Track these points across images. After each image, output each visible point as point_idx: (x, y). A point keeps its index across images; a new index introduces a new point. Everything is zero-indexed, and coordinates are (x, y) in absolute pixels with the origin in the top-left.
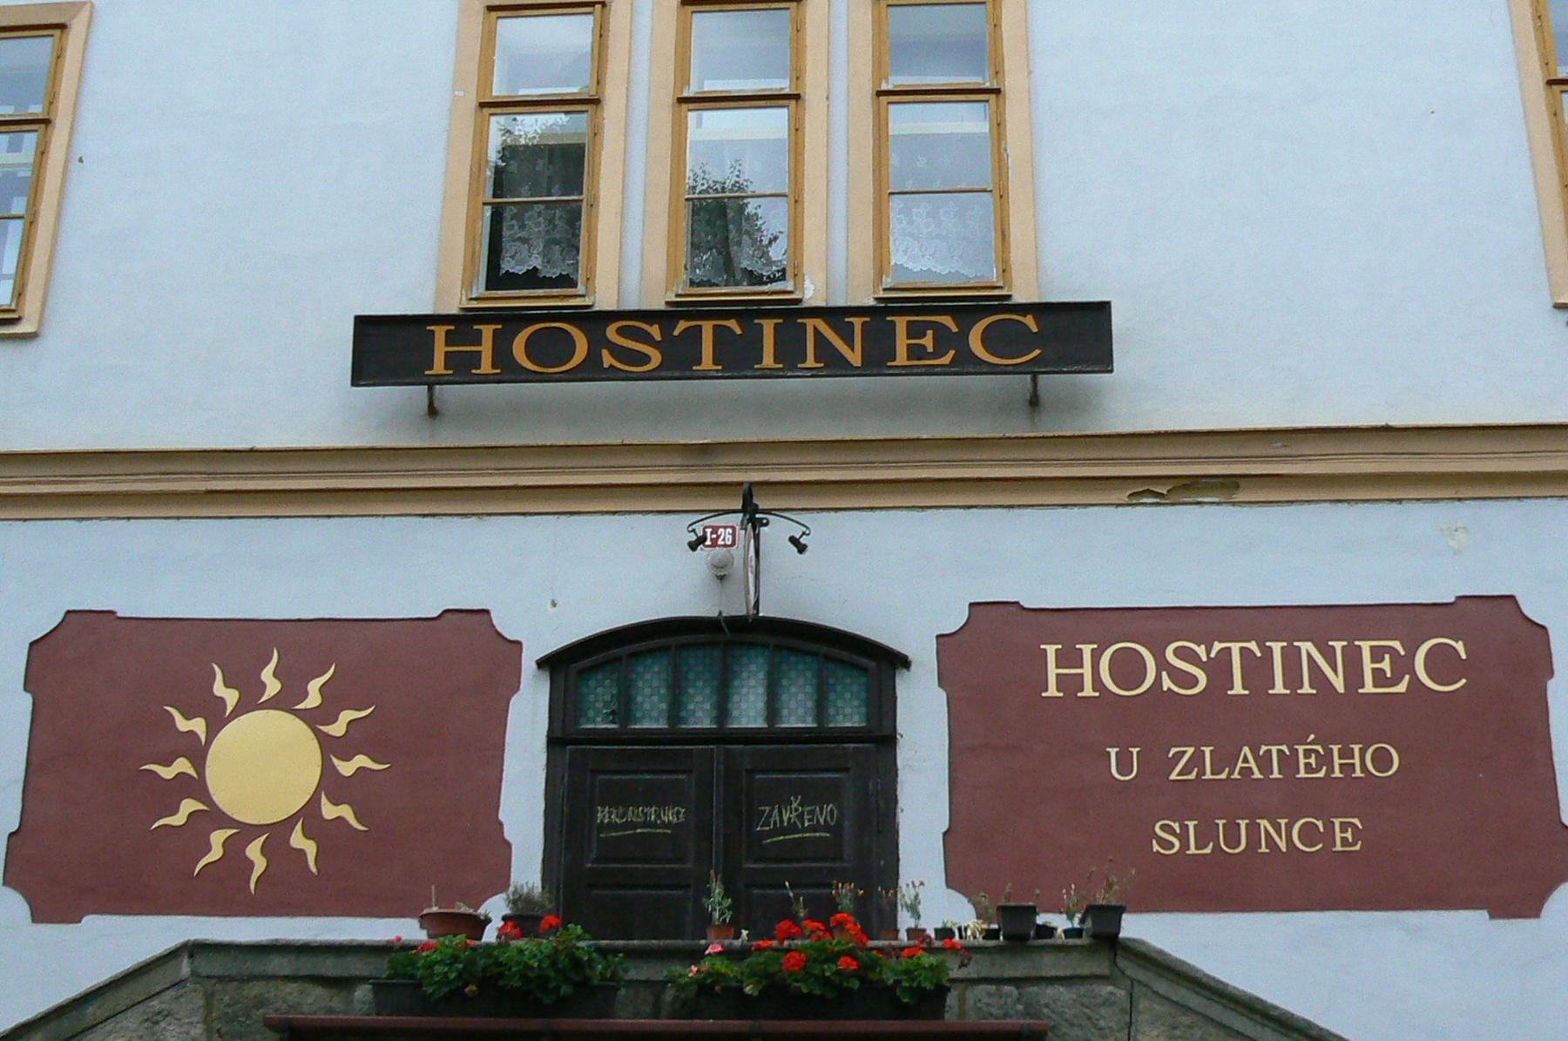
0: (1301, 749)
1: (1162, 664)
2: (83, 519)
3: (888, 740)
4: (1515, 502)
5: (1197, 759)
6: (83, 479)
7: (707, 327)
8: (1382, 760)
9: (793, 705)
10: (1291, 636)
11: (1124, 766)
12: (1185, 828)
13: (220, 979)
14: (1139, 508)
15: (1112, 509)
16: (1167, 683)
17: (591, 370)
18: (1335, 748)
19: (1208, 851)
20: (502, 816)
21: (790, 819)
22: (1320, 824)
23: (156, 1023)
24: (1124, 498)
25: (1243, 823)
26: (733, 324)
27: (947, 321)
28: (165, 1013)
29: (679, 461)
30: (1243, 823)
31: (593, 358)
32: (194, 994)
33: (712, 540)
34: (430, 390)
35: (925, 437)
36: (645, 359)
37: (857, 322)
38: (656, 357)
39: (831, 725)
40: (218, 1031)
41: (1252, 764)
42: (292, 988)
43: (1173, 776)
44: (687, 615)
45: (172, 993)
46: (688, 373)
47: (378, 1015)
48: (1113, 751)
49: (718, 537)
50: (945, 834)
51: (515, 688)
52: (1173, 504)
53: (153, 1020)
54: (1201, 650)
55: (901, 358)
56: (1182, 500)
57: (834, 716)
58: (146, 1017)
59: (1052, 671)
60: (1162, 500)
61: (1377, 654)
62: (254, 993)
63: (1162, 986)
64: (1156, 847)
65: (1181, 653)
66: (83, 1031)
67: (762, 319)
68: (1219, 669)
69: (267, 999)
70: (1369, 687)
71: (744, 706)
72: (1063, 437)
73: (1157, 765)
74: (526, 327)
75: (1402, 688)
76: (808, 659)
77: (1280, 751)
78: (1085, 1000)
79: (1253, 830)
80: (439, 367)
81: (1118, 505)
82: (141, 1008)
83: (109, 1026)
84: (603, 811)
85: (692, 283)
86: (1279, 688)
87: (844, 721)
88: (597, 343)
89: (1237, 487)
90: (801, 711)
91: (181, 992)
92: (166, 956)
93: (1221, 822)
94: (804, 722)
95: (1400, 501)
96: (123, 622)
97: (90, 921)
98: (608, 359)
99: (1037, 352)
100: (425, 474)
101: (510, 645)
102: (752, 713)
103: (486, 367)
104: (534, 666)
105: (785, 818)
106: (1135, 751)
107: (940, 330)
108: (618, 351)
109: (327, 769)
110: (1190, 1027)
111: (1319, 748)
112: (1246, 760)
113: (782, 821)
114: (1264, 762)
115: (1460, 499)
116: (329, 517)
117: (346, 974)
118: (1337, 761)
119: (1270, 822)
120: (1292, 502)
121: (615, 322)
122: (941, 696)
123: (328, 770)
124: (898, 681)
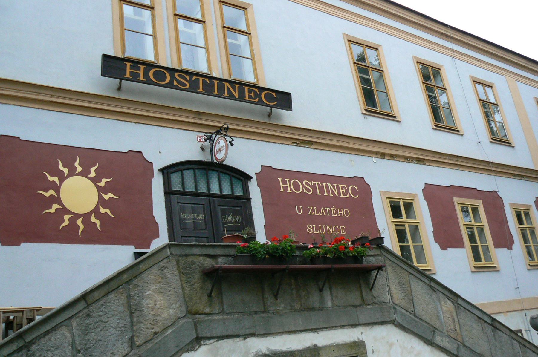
0: (332, 209)
1: (303, 186)
2: (4, 103)
3: (249, 199)
4: (361, 156)
5: (313, 210)
6: (7, 89)
7: (201, 79)
8: (346, 212)
9: (225, 188)
10: (326, 182)
11: (299, 211)
12: (313, 227)
13: (180, 255)
14: (293, 146)
15: (288, 145)
16: (305, 191)
17: (170, 85)
18: (338, 209)
19: (318, 232)
20: (154, 215)
21: (230, 220)
22: (338, 227)
23: (163, 270)
24: (290, 143)
25: (324, 226)
26: (207, 80)
27: (256, 90)
28: (165, 267)
29: (192, 116)
30: (324, 226)
31: (171, 82)
32: (172, 261)
33: (199, 139)
34: (121, 82)
35: (252, 120)
36: (185, 85)
37: (237, 86)
38: (188, 86)
39: (235, 194)
40: (182, 273)
41: (324, 212)
42: (201, 258)
43: (309, 214)
44: (191, 160)
45: (165, 261)
46: (196, 91)
47: (234, 264)
48: (296, 206)
49: (201, 139)
50: (264, 225)
51: (153, 176)
52: (300, 146)
53: (162, 269)
54: (310, 183)
55: (247, 98)
56: (302, 146)
57: (236, 192)
58: (159, 268)
59: (281, 185)
60: (298, 145)
61: (343, 188)
62: (191, 260)
63: (389, 257)
64: (308, 231)
65: (306, 183)
66: (140, 273)
67: (215, 80)
68: (314, 187)
69: (195, 262)
70: (342, 196)
71: (214, 187)
72: (273, 124)
73: (306, 211)
74: (154, 68)
75: (347, 196)
76: (228, 176)
77: (328, 209)
78: (377, 261)
79: (326, 227)
80: (128, 75)
81: (289, 145)
82: (158, 265)
83: (148, 272)
84: (183, 215)
85: (374, 80)
86: (326, 194)
87: (238, 194)
88: (173, 77)
89: (312, 144)
90: (228, 190)
91: (169, 260)
92: (163, 248)
93: (320, 226)
94: (229, 193)
95: (342, 153)
96: (22, 141)
97: (23, 245)
98: (175, 83)
99: (276, 103)
100: (122, 107)
101: (149, 163)
102: (216, 190)
103: (142, 78)
104: (158, 170)
105: (229, 219)
106: (301, 207)
107: (255, 92)
108: (178, 81)
109: (100, 197)
110: (395, 267)
111: (335, 209)
112: (322, 211)
113: (228, 220)
114: (326, 211)
115: (352, 154)
116: (90, 116)
117: (216, 254)
118: (339, 213)
119: (329, 226)
120: (322, 150)
121: (178, 72)
122: (259, 189)
123: (100, 198)
124: (249, 184)
